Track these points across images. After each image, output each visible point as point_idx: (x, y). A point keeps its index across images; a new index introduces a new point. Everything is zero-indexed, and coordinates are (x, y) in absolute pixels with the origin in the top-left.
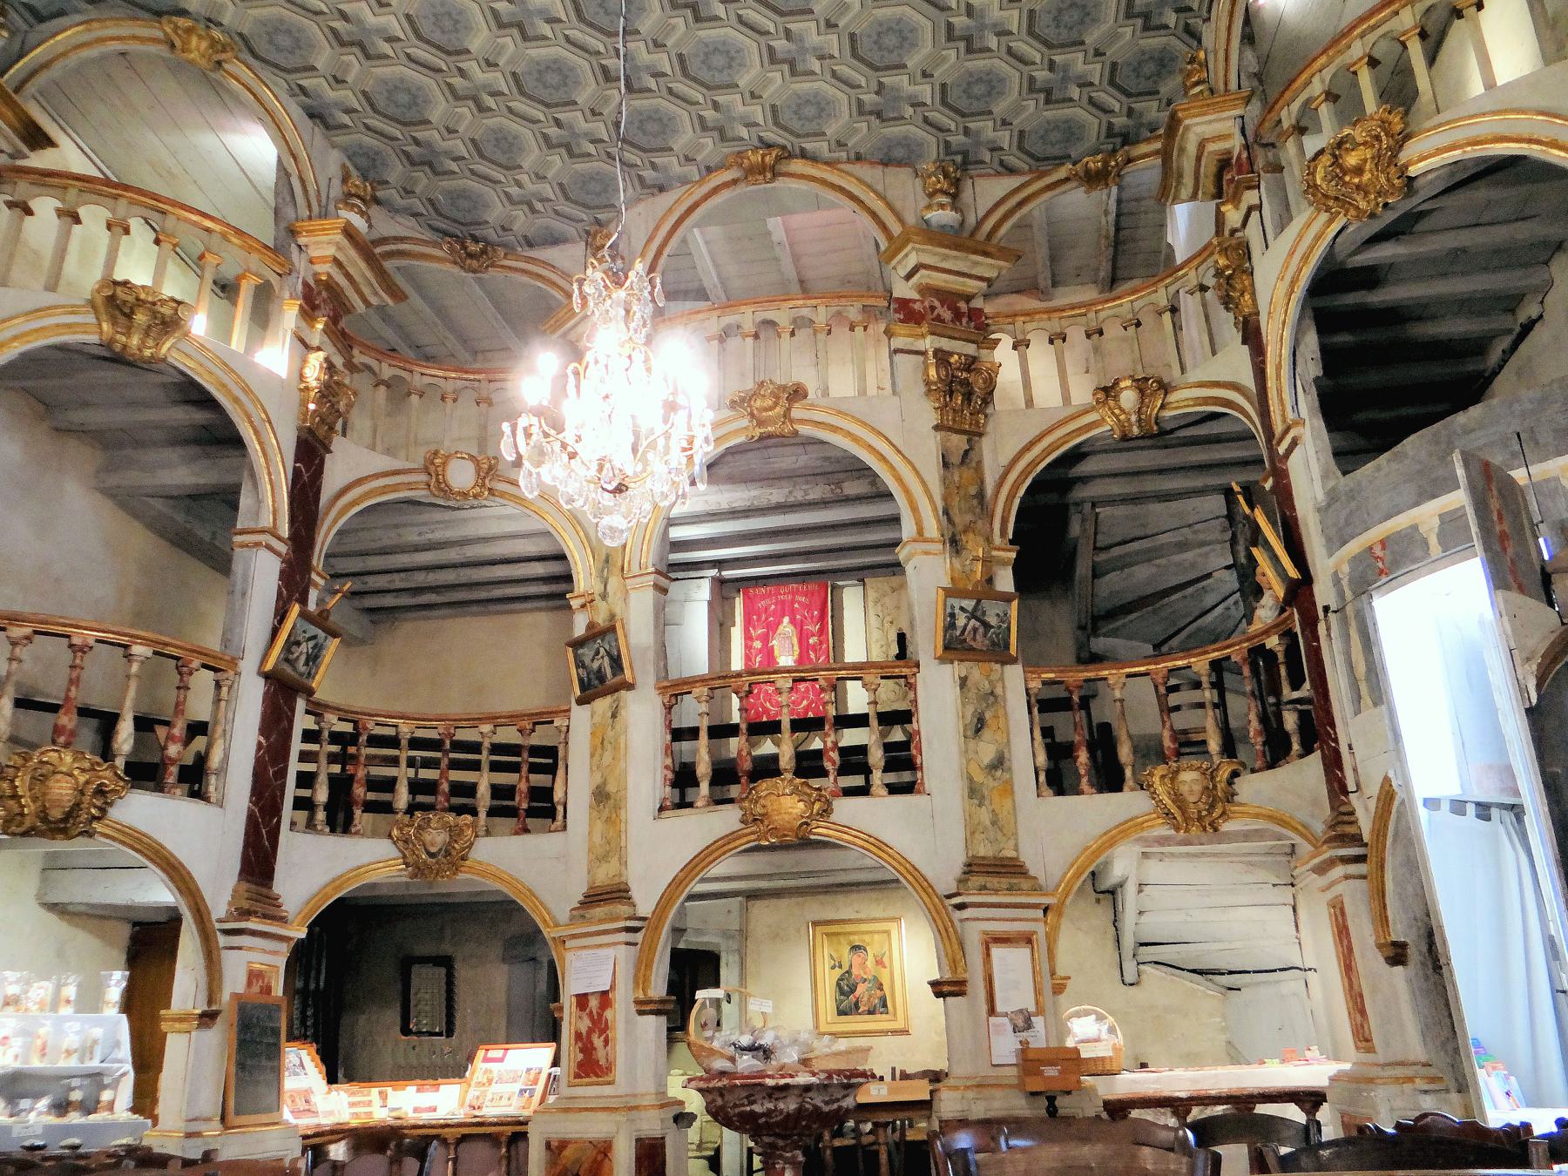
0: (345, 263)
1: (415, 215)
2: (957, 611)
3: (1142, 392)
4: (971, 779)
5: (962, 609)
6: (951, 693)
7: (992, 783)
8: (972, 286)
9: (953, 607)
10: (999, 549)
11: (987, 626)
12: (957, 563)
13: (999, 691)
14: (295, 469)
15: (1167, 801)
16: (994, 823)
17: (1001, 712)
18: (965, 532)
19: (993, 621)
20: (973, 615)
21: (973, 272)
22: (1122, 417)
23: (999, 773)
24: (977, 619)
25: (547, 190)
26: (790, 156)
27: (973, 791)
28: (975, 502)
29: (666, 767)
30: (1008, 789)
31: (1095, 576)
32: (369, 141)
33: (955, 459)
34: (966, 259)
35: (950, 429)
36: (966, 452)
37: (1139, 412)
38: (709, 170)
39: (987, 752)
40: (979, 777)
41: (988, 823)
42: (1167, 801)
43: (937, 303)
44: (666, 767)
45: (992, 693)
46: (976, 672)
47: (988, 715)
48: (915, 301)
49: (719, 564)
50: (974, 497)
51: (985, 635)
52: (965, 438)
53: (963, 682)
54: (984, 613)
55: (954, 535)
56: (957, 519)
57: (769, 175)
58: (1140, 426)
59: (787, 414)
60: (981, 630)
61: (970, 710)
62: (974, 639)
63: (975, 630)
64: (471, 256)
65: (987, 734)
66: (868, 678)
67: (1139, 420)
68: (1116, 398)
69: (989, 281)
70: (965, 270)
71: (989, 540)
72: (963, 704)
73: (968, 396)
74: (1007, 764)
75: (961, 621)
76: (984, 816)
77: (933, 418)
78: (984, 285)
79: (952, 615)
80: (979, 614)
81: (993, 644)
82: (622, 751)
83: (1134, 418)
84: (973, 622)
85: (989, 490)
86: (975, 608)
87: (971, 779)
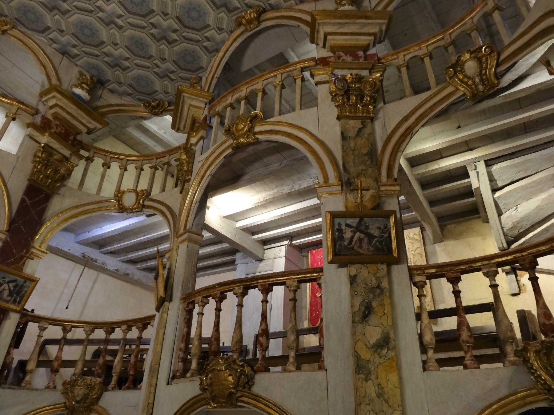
0: (64, 107)
1: (130, 95)
2: (343, 227)
3: (479, 60)
4: (357, 357)
5: (348, 225)
6: (345, 288)
7: (377, 360)
8: (364, 40)
9: (339, 225)
10: (384, 185)
11: (371, 237)
12: (351, 197)
13: (385, 284)
14: (23, 201)
15: (544, 376)
16: (379, 396)
17: (387, 301)
18: (358, 177)
19: (376, 233)
20: (357, 229)
21: (363, 31)
22: (470, 82)
23: (384, 352)
24: (361, 232)
25: (169, 65)
26: (264, 11)
27: (361, 368)
28: (366, 158)
29: (180, 350)
30: (396, 365)
31: (500, 214)
32: (86, 59)
33: (352, 133)
34: (355, 24)
35: (347, 117)
36: (360, 129)
37: (480, 74)
38: (232, 32)
39: (374, 334)
40: (365, 355)
41: (374, 395)
42: (544, 376)
43: (342, 54)
44: (180, 350)
45: (379, 287)
46: (365, 273)
47: (374, 304)
48: (330, 57)
49: (290, 237)
50: (367, 154)
51: (370, 243)
52: (360, 121)
53: (353, 280)
54: (367, 227)
55: (348, 179)
56: (352, 170)
57: (256, 23)
58: (483, 84)
59: (251, 129)
60: (366, 240)
61: (358, 301)
62: (360, 247)
63: (360, 240)
64: (154, 107)
65: (373, 319)
66: (288, 283)
67: (482, 80)
68: (462, 71)
69: (374, 34)
70: (357, 31)
71: (377, 180)
72: (352, 297)
73: (361, 97)
74: (392, 344)
75: (348, 235)
76: (371, 388)
77: (335, 112)
78: (372, 38)
79: (340, 231)
80: (362, 228)
81: (377, 249)
82: (184, 339)
83: (477, 80)
84: (358, 235)
85: (379, 149)
86: (359, 224)
87: (357, 357)
